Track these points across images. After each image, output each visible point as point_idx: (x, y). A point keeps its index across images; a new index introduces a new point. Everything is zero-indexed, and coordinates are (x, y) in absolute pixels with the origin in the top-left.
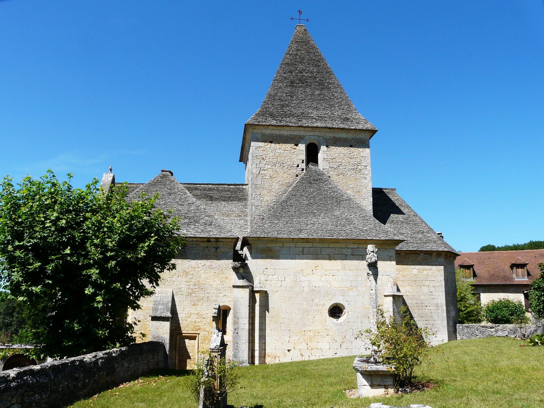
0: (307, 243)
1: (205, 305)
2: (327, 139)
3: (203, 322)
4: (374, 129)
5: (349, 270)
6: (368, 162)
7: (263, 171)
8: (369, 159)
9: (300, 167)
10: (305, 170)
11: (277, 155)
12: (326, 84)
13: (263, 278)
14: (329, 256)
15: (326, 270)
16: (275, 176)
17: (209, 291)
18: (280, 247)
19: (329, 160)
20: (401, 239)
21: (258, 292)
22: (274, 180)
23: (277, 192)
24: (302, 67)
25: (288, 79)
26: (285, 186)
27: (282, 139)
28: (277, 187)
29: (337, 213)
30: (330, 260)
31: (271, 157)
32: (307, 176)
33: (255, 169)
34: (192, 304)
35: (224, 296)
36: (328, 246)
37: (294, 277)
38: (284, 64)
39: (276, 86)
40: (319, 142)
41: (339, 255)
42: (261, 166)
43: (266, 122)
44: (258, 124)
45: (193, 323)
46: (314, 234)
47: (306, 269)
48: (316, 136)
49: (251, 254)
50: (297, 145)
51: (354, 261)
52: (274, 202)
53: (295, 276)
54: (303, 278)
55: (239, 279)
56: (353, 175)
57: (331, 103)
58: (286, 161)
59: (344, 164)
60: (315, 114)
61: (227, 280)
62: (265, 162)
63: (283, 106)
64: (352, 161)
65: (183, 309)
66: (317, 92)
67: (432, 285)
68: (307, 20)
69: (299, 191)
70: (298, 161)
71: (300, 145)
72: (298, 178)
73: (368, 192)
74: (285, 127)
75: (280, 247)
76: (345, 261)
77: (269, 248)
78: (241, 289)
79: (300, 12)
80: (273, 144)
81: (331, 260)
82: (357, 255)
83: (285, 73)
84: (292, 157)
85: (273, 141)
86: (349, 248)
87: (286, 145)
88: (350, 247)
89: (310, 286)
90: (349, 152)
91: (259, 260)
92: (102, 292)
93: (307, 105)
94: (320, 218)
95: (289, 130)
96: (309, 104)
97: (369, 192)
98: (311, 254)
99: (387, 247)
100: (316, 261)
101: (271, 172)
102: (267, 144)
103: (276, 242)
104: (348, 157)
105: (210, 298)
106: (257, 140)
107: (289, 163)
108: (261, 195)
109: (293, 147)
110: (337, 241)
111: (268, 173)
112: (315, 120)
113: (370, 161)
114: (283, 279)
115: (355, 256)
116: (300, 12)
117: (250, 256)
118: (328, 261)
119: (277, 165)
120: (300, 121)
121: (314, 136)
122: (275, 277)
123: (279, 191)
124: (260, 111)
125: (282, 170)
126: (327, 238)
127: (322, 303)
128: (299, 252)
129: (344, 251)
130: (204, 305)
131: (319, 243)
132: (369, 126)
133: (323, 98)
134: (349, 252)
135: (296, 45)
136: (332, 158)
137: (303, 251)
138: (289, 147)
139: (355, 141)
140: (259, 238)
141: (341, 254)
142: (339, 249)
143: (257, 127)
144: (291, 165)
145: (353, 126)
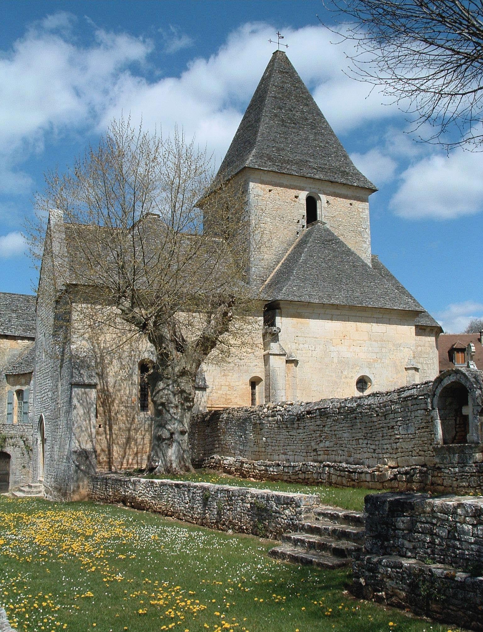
5: (375, 341)
8: (369, 221)
9: (300, 223)
11: (277, 207)
15: (354, 340)
25: (279, 117)
34: (223, 374)
45: (224, 396)
53: (325, 346)
54: (332, 348)
58: (286, 215)
67: (425, 362)
72: (298, 236)
88: (375, 316)
101: (271, 226)
107: (290, 218)
114: (313, 349)
122: (306, 346)
127: (350, 376)
130: (234, 375)
136: (333, 216)
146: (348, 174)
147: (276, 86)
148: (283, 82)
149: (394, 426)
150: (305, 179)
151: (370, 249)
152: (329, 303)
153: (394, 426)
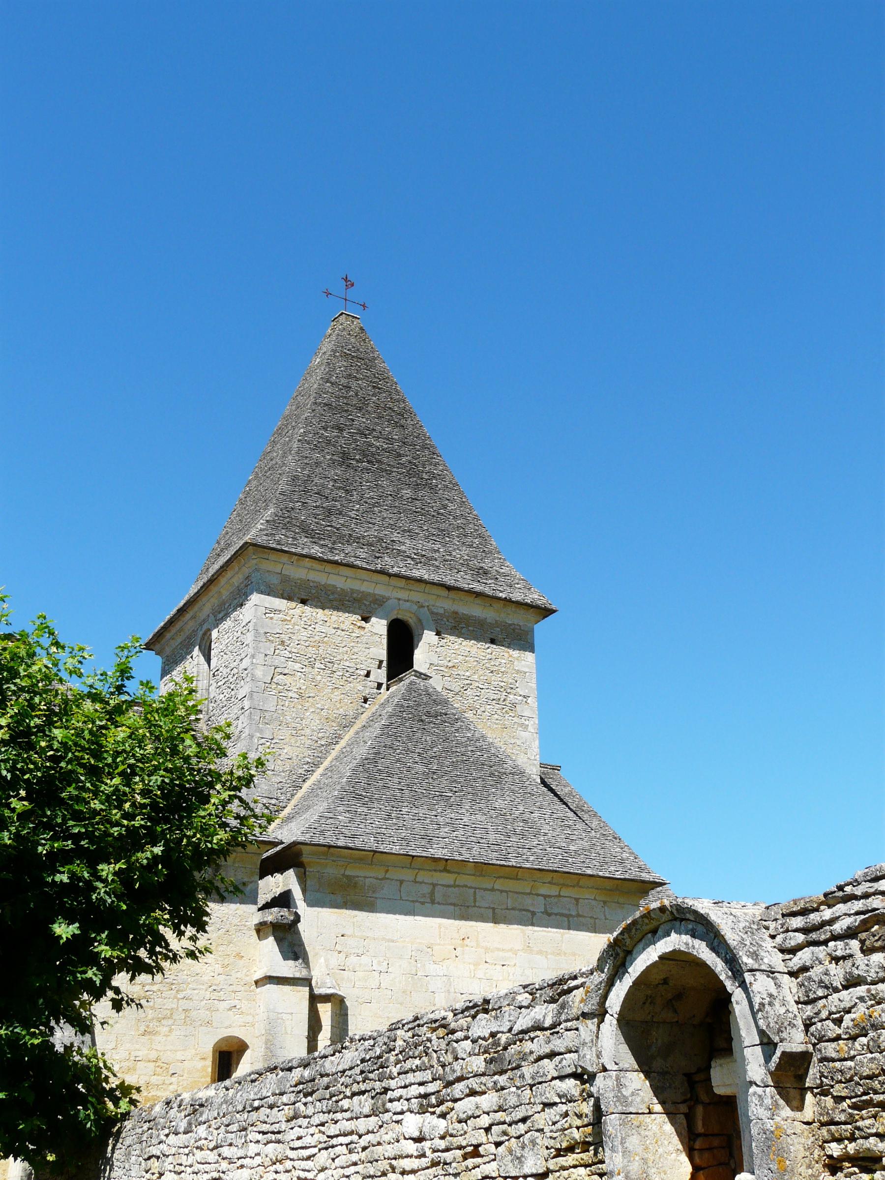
0: (445, 874)
1: (178, 1033)
2: (437, 614)
3: (171, 1087)
4: (548, 606)
5: (540, 952)
6: (531, 687)
7: (281, 676)
8: (534, 681)
9: (372, 677)
10: (384, 686)
11: (317, 638)
12: (425, 476)
13: (335, 960)
14: (494, 913)
15: (487, 950)
16: (311, 695)
17: (189, 992)
18: (377, 879)
19: (441, 669)
20: (657, 881)
21: (326, 998)
22: (307, 704)
23: (315, 738)
24: (364, 420)
25: (334, 446)
26: (334, 725)
27: (331, 597)
28: (316, 724)
29: (499, 803)
30: (495, 923)
31: (303, 643)
32: (411, 703)
33: (262, 668)
34: (142, 1028)
35: (230, 1009)
36: (489, 886)
37: (410, 963)
38: (320, 403)
39: (306, 457)
40: (420, 620)
41: (517, 912)
42: (276, 663)
43: (296, 545)
44: (279, 547)
46: (463, 851)
47: (439, 944)
48: (413, 602)
49: (304, 891)
50: (366, 619)
51: (550, 929)
52: (308, 763)
53: (413, 961)
54: (432, 968)
55: (285, 958)
56: (496, 716)
57: (443, 526)
58: (339, 657)
59: (477, 684)
60: (407, 546)
61: (241, 962)
62: (288, 655)
63: (329, 512)
64: (495, 679)
65: (113, 1045)
66: (407, 493)
68: (364, 306)
69: (399, 739)
70: (370, 661)
71: (374, 620)
72: (367, 706)
73: (531, 762)
74: (342, 568)
75: (377, 879)
76: (530, 928)
77: (349, 877)
78: (287, 989)
79: (349, 283)
80: (307, 609)
81: (499, 923)
82: (556, 914)
83: (325, 428)
84: (356, 650)
85: (308, 600)
86: (538, 895)
87: (340, 614)
89: (449, 991)
90: (489, 656)
91: (325, 909)
92: (104, 936)
93: (387, 520)
94: (464, 811)
95: (351, 577)
96: (390, 518)
97: (534, 765)
98: (451, 904)
99: (621, 900)
100: (463, 923)
101: (302, 681)
102: (294, 604)
103: (371, 864)
104: (487, 668)
105: (193, 1014)
106: (269, 592)
107: (347, 664)
108: (273, 741)
109: (359, 624)
110: (515, 873)
111: (296, 683)
112: (412, 563)
113: (534, 686)
115: (553, 917)
116: (349, 283)
117: (301, 896)
118: (492, 925)
119: (318, 665)
120: (378, 558)
121: (408, 601)
123: (320, 735)
124: (277, 516)
125: (329, 679)
126: (494, 862)
128: (424, 896)
129: (528, 902)
130: (174, 1033)
131: (474, 875)
132: (533, 597)
133: (422, 509)
134: (539, 905)
135: (345, 363)
136: (450, 664)
137: (432, 893)
138: (347, 623)
139: (502, 630)
140: (332, 850)
141: (520, 910)
142: (516, 895)
143: (273, 556)
144: (351, 670)
145: (501, 592)
146: (486, 573)
147: (332, 384)
148: (349, 376)
149: (480, 1145)
150: (385, 578)
151: (537, 742)
152: (424, 854)
153: (480, 1145)
